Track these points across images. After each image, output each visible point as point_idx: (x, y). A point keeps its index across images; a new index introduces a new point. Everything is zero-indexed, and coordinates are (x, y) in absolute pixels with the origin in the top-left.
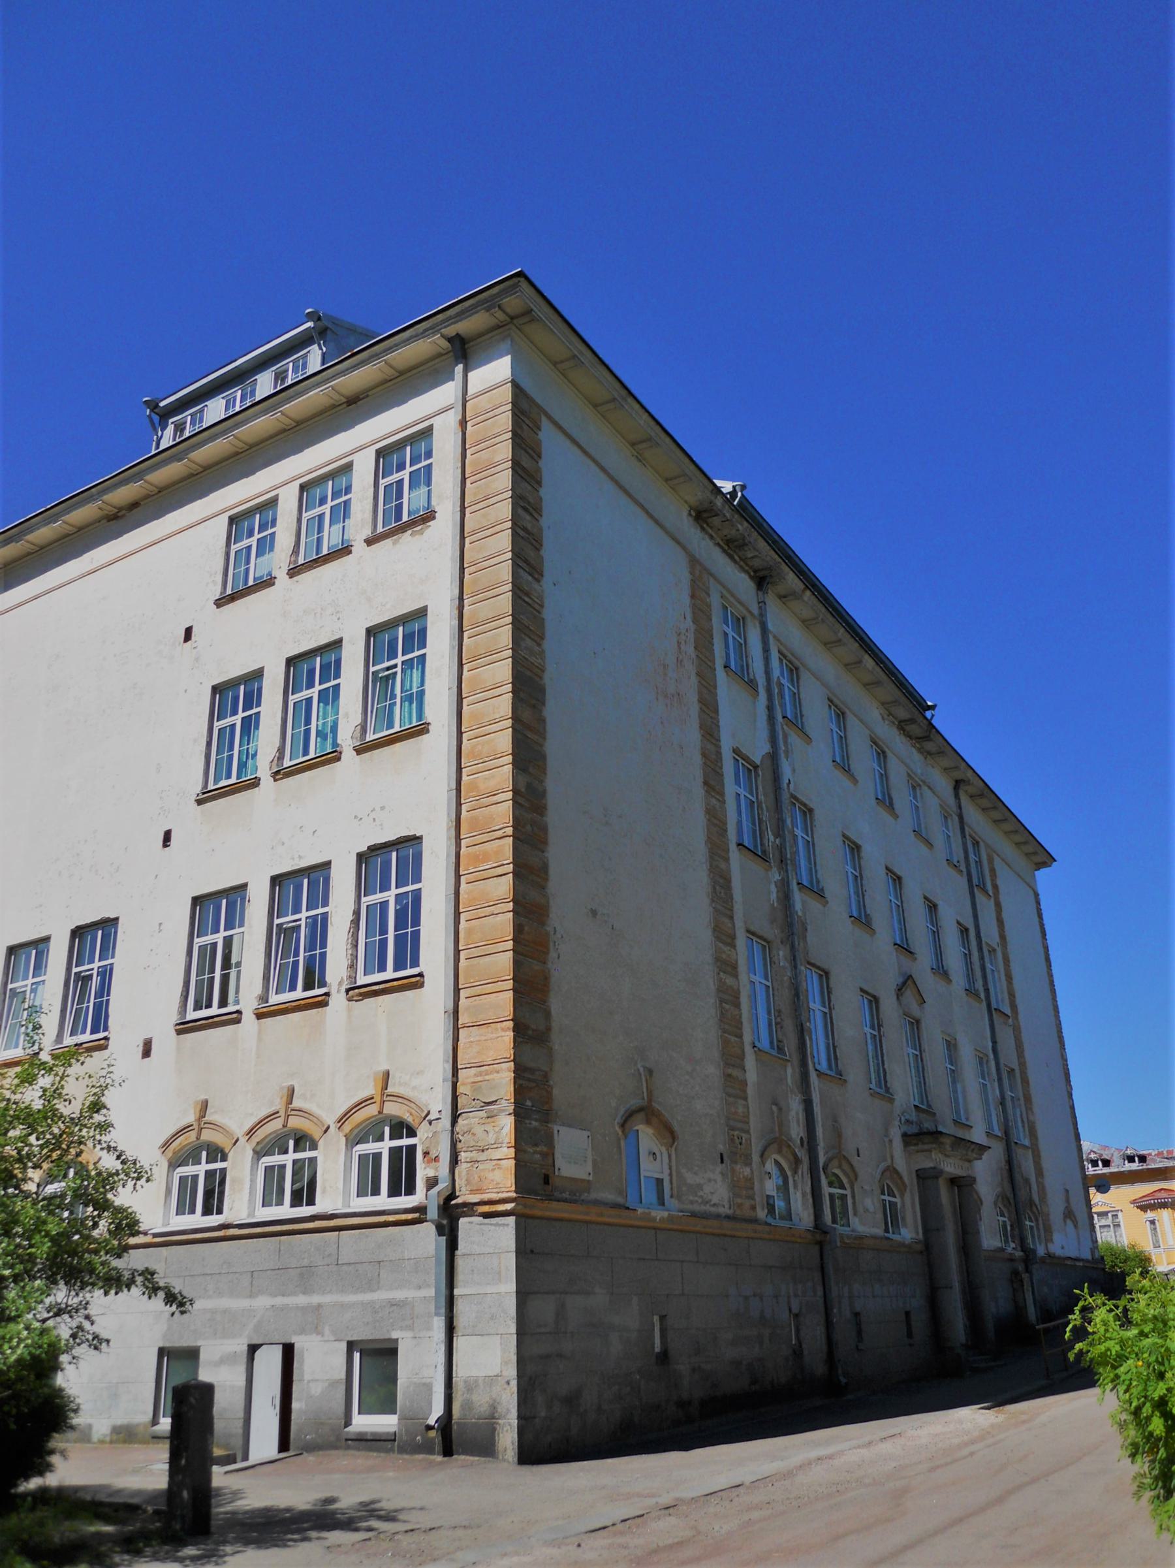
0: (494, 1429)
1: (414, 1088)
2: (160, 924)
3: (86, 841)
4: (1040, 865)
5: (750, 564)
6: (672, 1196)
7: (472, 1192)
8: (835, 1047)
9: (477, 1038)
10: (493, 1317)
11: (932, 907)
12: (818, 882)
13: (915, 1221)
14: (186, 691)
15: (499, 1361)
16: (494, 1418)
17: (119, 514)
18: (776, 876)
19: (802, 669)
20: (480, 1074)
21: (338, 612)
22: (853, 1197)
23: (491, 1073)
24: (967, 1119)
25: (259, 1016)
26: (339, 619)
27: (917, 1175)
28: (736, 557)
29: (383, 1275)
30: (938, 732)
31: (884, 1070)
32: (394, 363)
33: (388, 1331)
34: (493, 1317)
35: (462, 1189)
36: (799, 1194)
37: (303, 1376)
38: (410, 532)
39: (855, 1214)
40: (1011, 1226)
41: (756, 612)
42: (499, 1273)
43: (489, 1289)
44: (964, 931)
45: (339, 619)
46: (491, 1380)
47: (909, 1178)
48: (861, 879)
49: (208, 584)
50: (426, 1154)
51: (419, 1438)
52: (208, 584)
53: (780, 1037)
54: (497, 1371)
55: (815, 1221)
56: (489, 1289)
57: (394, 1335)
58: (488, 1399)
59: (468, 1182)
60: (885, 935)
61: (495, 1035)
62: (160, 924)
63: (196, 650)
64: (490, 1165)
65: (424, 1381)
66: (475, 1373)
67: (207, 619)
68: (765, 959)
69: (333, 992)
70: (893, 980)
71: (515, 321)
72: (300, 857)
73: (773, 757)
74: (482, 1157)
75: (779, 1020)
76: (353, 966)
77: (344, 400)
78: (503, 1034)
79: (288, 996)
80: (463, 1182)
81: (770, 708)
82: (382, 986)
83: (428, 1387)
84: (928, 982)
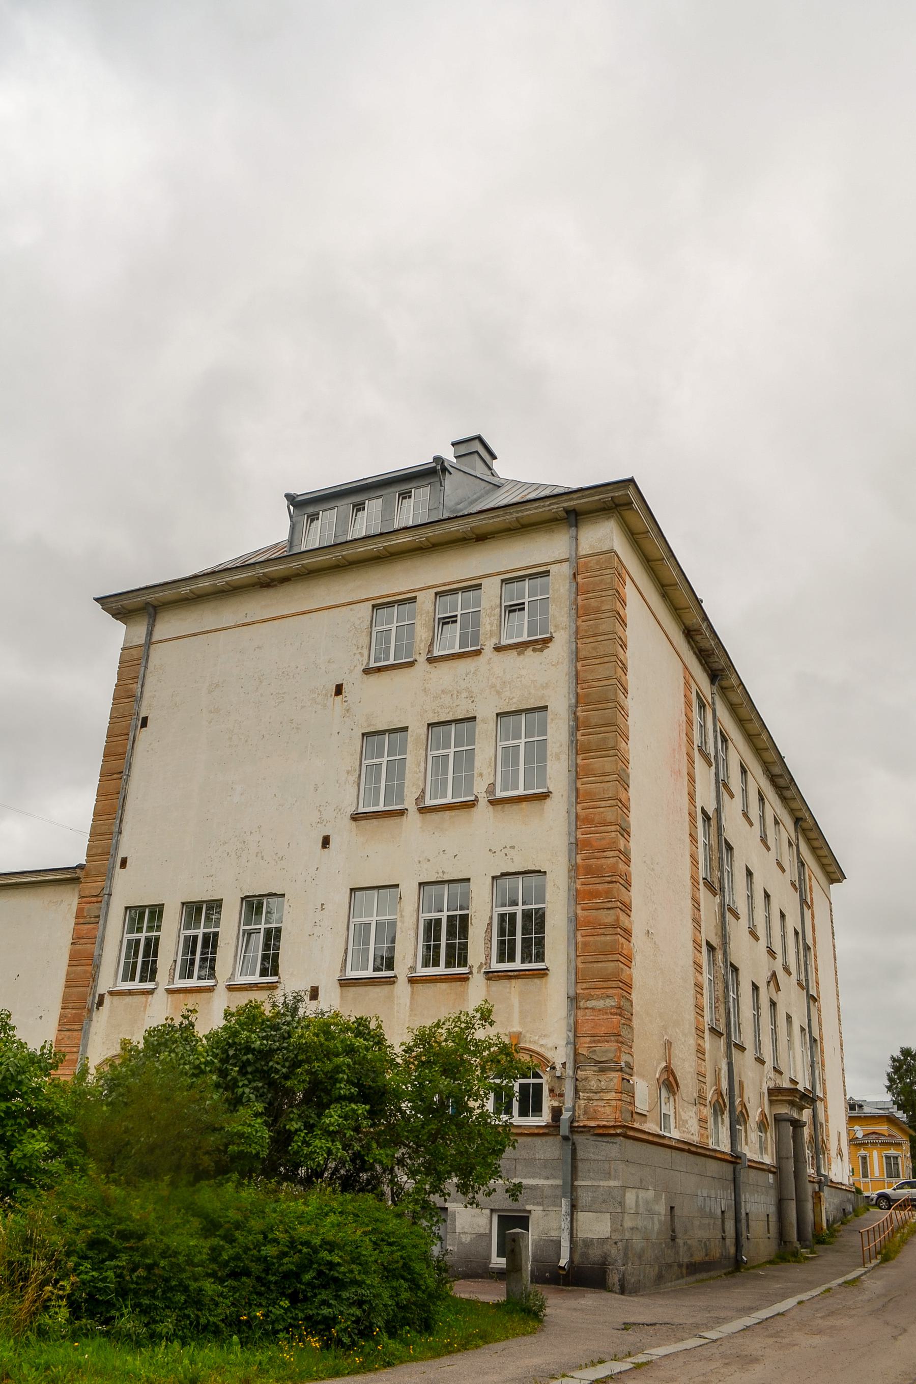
0: (606, 1272)
1: (542, 1045)
2: (323, 905)
3: (251, 833)
4: (832, 881)
5: (710, 665)
6: (676, 1128)
7: (589, 1119)
8: (739, 1024)
9: (592, 1017)
10: (604, 1201)
11: (783, 916)
12: (734, 903)
13: (772, 1152)
14: (338, 733)
15: (609, 1229)
16: (606, 1265)
17: (272, 584)
18: (718, 899)
19: (729, 741)
20: (594, 1042)
21: (472, 697)
22: (746, 1132)
23: (603, 1042)
24: (795, 1077)
25: (412, 981)
26: (472, 702)
27: (775, 1118)
28: (704, 662)
29: (519, 1167)
30: (795, 784)
31: (759, 1041)
32: (521, 521)
33: (523, 1205)
34: (604, 1201)
35: (582, 1117)
36: (725, 1128)
37: (455, 1229)
38: (531, 648)
39: (747, 1144)
40: (812, 1157)
41: (710, 702)
42: (609, 1173)
43: (602, 1183)
44: (796, 933)
45: (472, 702)
46: (603, 1241)
47: (770, 1120)
48: (752, 899)
49: (355, 654)
50: (551, 1091)
51: (547, 1274)
52: (355, 654)
53: (718, 1017)
54: (608, 1235)
55: (731, 1147)
56: (602, 1183)
57: (528, 1208)
58: (600, 1252)
59: (585, 1113)
60: (763, 942)
61: (605, 1017)
62: (323, 905)
63: (346, 703)
64: (601, 1103)
65: (551, 1238)
66: (590, 1236)
67: (355, 684)
68: (709, 961)
69: (475, 970)
70: (767, 975)
71: (618, 508)
72: (443, 872)
73: (718, 811)
74: (597, 1096)
75: (717, 1004)
76: (488, 956)
77: (474, 536)
78: (612, 1017)
79: (431, 971)
80: (581, 1112)
81: (717, 774)
82: (516, 973)
83: (558, 1244)
84: (781, 975)
